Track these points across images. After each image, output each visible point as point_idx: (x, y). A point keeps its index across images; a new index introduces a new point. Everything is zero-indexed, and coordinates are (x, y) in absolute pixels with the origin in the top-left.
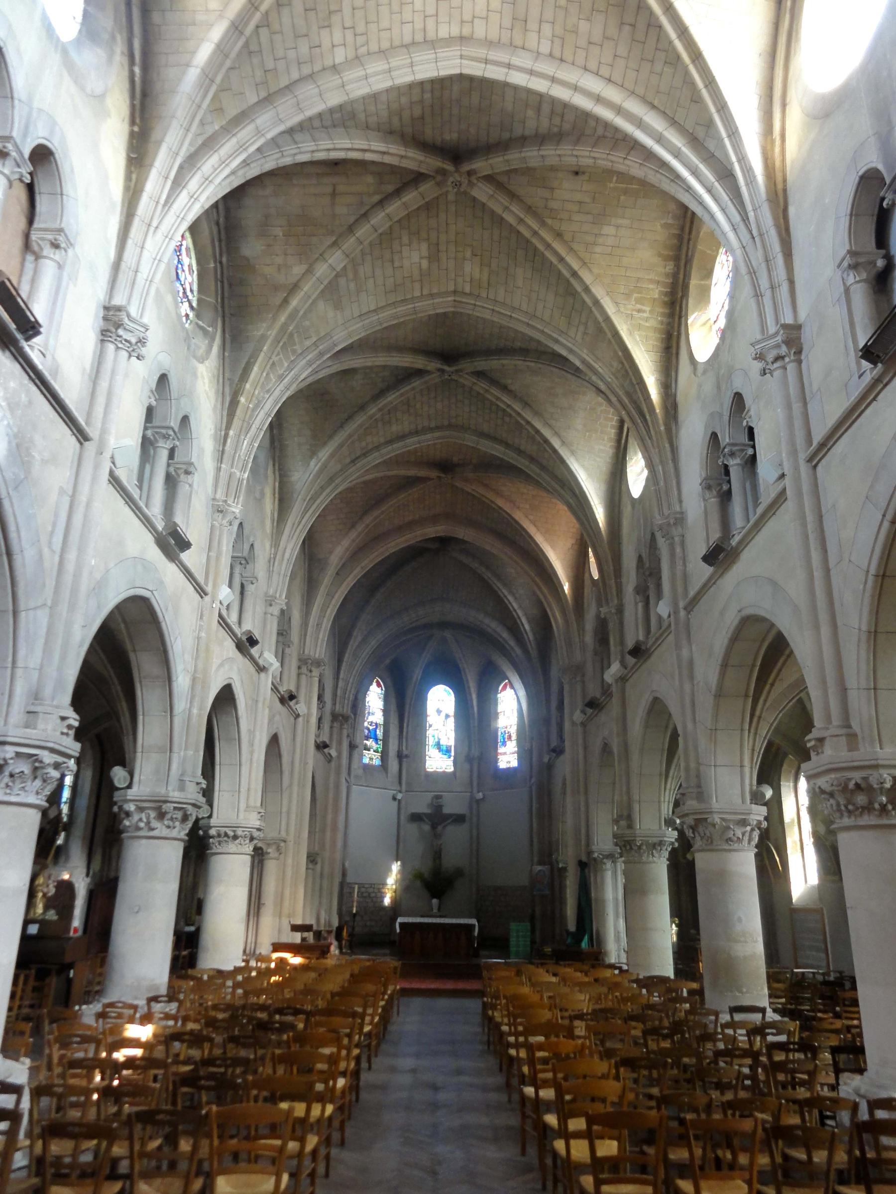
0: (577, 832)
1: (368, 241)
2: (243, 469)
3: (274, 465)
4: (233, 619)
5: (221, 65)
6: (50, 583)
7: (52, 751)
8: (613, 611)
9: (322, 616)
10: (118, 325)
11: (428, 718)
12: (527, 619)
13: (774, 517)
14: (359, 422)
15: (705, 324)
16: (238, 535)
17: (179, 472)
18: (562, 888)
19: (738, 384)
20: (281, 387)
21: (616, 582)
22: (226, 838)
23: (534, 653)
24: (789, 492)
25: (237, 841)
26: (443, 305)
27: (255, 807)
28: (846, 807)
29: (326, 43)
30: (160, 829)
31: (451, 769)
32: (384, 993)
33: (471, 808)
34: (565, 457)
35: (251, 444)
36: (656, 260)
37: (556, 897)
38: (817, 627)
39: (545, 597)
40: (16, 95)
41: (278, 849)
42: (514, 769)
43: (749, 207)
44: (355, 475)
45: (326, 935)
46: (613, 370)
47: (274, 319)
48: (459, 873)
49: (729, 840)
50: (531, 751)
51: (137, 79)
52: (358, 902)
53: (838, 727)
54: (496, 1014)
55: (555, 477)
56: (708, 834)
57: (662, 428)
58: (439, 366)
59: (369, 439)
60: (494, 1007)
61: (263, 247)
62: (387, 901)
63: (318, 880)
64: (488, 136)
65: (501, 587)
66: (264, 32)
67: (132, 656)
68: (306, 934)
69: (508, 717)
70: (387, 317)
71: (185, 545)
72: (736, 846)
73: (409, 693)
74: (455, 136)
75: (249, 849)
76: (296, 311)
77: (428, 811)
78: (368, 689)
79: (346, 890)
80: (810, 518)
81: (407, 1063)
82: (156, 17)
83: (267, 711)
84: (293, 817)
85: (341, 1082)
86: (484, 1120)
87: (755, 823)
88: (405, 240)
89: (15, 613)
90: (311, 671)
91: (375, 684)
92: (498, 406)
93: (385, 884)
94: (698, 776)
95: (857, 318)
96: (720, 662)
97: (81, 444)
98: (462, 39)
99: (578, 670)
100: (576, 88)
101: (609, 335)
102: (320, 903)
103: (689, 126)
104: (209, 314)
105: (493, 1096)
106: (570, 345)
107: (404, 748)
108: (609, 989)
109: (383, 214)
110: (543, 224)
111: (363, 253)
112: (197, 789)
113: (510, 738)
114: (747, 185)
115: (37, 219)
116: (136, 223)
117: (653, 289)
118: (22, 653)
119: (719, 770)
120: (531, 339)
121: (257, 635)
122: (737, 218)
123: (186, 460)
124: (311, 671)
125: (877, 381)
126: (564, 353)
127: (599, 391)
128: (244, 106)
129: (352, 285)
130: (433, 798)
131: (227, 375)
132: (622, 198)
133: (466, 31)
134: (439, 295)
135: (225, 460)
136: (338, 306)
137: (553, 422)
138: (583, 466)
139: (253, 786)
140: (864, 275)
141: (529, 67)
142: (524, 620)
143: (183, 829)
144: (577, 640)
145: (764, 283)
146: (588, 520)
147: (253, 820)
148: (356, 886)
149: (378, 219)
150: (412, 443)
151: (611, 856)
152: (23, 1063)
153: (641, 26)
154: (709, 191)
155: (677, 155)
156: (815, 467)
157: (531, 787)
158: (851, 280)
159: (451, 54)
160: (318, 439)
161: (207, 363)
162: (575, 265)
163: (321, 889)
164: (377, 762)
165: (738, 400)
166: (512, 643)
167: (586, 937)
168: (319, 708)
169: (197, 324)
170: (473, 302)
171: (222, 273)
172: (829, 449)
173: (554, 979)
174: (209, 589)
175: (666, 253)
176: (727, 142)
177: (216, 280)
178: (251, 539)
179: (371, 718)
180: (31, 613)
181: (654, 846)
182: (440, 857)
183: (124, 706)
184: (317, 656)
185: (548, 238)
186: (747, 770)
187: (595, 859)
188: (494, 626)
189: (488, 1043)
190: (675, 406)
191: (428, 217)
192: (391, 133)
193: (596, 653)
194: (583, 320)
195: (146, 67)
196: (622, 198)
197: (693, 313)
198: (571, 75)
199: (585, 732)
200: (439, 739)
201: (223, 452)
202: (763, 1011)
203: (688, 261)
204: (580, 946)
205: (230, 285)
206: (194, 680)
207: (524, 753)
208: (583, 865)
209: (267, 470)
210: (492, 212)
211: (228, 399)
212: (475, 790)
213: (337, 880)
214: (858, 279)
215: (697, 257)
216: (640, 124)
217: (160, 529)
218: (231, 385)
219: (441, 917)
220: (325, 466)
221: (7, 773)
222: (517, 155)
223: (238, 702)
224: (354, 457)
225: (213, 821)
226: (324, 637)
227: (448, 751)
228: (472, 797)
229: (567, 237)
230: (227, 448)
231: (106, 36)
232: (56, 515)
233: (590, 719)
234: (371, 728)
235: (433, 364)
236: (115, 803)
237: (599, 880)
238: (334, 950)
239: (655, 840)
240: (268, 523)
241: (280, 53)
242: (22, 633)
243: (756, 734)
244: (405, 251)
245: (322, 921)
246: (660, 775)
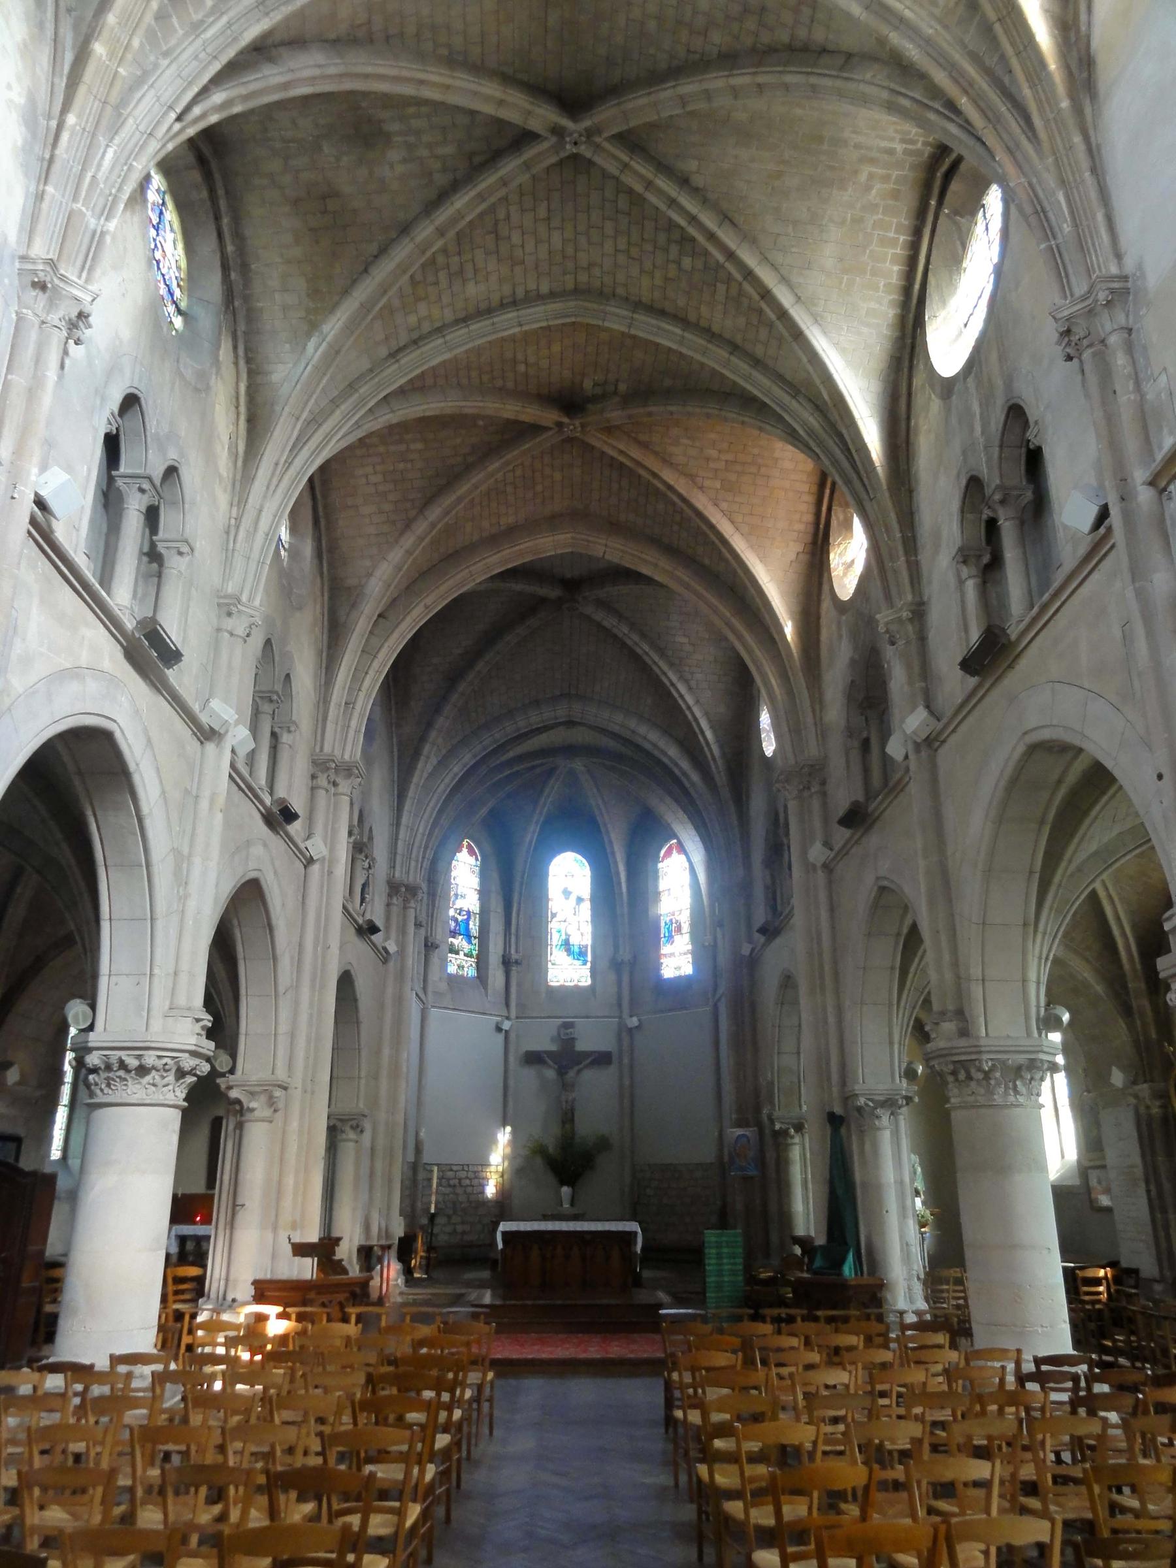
3: (235, 348)
8: (905, 614)
11: (550, 903)
12: (710, 721)
14: (397, 260)
22: (122, 1073)
23: (721, 778)
25: (148, 1078)
31: (586, 981)
33: (620, 1040)
34: (803, 326)
41: (271, 1102)
42: (688, 977)
46: (937, 12)
48: (603, 1144)
57: (1065, 104)
59: (423, 309)
62: (490, 1191)
63: (366, 1162)
65: (665, 668)
69: (677, 898)
71: (172, 656)
79: (421, 1175)
84: (301, 1043)
90: (335, 784)
91: (465, 850)
97: (202, 743)
102: (371, 1199)
107: (513, 951)
112: (197, 1028)
113: (679, 929)
124: (335, 784)
135: (53, 177)
137: (779, 258)
138: (836, 345)
139: (185, 966)
142: (704, 724)
144: (810, 720)
146: (847, 450)
148: (435, 1169)
151: (890, 1103)
157: (716, 1007)
163: (372, 1174)
164: (470, 972)
167: (850, 1257)
179: (459, 904)
182: (572, 1120)
184: (347, 757)
187: (859, 1110)
188: (653, 737)
199: (830, 883)
201: (51, 160)
204: (840, 1274)
207: (703, 951)
211: (69, 57)
219: (576, 1218)
223: (136, 779)
224: (394, 345)
227: (582, 954)
233: (844, 852)
234: (460, 918)
237: (868, 1147)
239: (1021, 1059)
245: (375, 1230)
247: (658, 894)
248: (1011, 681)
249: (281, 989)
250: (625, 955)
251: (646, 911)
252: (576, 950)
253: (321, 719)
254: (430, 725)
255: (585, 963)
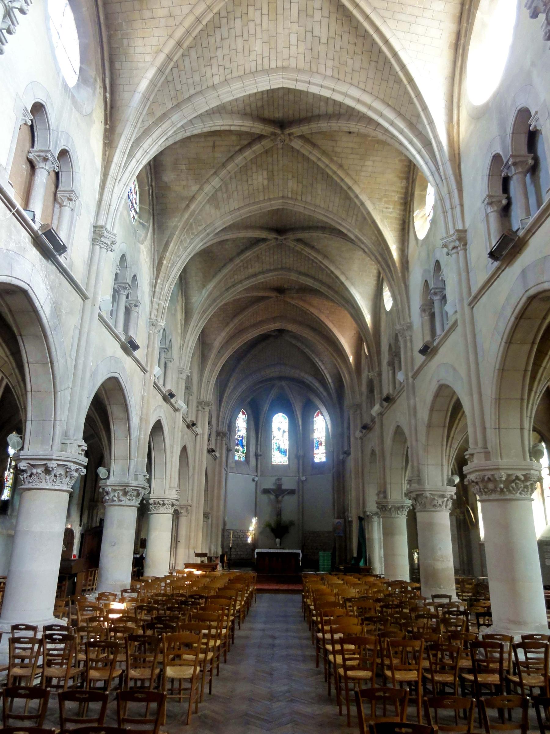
0: (358, 500)
1: (234, 171)
2: (166, 301)
3: (182, 293)
4: (160, 383)
5: (153, 90)
6: (71, 376)
7: (75, 463)
8: (376, 375)
9: (210, 377)
10: (101, 236)
13: (454, 332)
15: (423, 217)
16: (163, 336)
17: (131, 305)
18: (351, 531)
19: (438, 256)
20: (186, 254)
21: (378, 359)
23: (334, 395)
24: (459, 322)
25: (165, 507)
26: (277, 204)
27: (174, 487)
28: (483, 490)
29: (209, 74)
30: (125, 501)
31: (286, 463)
32: (247, 590)
35: (170, 287)
36: (396, 179)
37: (346, 537)
38: (471, 395)
39: (339, 364)
40: (51, 128)
41: (187, 510)
42: (324, 462)
43: (440, 164)
44: (229, 297)
45: (214, 559)
47: (182, 216)
48: (292, 523)
49: (435, 505)
50: (333, 452)
51: (108, 100)
52: (233, 541)
53: (481, 448)
54: (308, 601)
55: (343, 297)
56: (423, 503)
57: (400, 275)
58: (275, 236)
59: (236, 277)
60: (307, 597)
61: (175, 176)
62: (250, 540)
64: (299, 114)
66: (175, 70)
67: (108, 408)
68: (203, 559)
70: (245, 213)
71: (62, 249)
72: (438, 509)
73: (261, 417)
74: (281, 115)
75: (171, 511)
76: (194, 211)
77: (274, 487)
78: (237, 416)
79: (226, 534)
80: (469, 336)
81: (260, 626)
82: (117, 65)
83: (180, 433)
84: (195, 492)
85: (224, 631)
86: (299, 652)
87: (449, 496)
88: (254, 169)
89: (55, 393)
90: (204, 409)
91: (241, 413)
92: (309, 257)
93: (248, 530)
94: (419, 471)
95: (492, 231)
96: (429, 408)
97: (84, 301)
98: (283, 68)
99: (358, 406)
100: (346, 95)
101: (370, 221)
103: (408, 116)
104: (145, 215)
105: (305, 642)
106: (348, 227)
108: (370, 587)
109: (242, 157)
110: (332, 160)
111: (231, 178)
112: (144, 479)
113: (321, 444)
114: (439, 151)
115: (60, 185)
116: (109, 178)
117: (394, 196)
118: (59, 413)
119: (429, 467)
120: (326, 223)
121: (174, 392)
122: (434, 169)
123: (135, 299)
124: (204, 409)
125: (498, 268)
126: (345, 231)
127: (364, 251)
128: (165, 110)
129: (225, 196)
130: (276, 480)
131: (156, 248)
132: (376, 145)
133: (286, 64)
134: (274, 199)
135: (156, 296)
136: (217, 207)
139: (173, 476)
140: (496, 208)
141: (321, 83)
143: (137, 501)
144: (357, 390)
145: (448, 206)
147: (173, 495)
149: (239, 159)
150: (261, 279)
152: (65, 620)
153: (381, 63)
154: (419, 152)
155: (402, 132)
156: (472, 308)
158: (489, 210)
159: (277, 77)
160: (207, 278)
161: (145, 243)
162: (350, 183)
164: (243, 459)
165: (438, 263)
166: (321, 389)
168: (209, 429)
169: (139, 221)
170: (293, 203)
171: (153, 192)
172: (479, 300)
173: (341, 582)
174: (148, 369)
175: (401, 175)
176: (428, 127)
177: (149, 195)
178: (170, 337)
179: (239, 433)
180: (63, 392)
181: (399, 508)
183: (103, 434)
185: (334, 168)
186: (445, 468)
187: (368, 516)
188: (309, 379)
189: (305, 617)
190: (407, 262)
191: (267, 157)
192: (245, 114)
193: (368, 397)
194: (356, 213)
195: (112, 93)
196: (376, 145)
197: (417, 210)
198: (343, 88)
200: (279, 445)
201: (155, 291)
202: (450, 597)
203: (414, 181)
204: (358, 565)
205: (157, 198)
206: (141, 419)
208: (361, 519)
209: (178, 296)
210: (303, 155)
212: (301, 475)
213: (221, 527)
214: (492, 210)
215: (418, 178)
216: (381, 115)
217: (123, 339)
218: (158, 254)
220: (210, 293)
221: (53, 475)
222: (316, 126)
223: (164, 429)
225: (151, 496)
226: (211, 388)
227: (285, 452)
228: (299, 479)
229: (346, 167)
230: (157, 290)
231: (92, 80)
232: (73, 339)
233: (365, 436)
234: (239, 439)
235: (271, 236)
236: (100, 487)
237: (370, 528)
238: (219, 567)
239: (399, 505)
240: (179, 326)
241: (184, 81)
242: (58, 403)
243: (451, 447)
244: (254, 176)
246: (402, 468)
247: (313, 430)
248: (395, 405)
249: (190, 476)
250: (301, 453)
251: (309, 436)
252: (283, 450)
253: (200, 388)
254: (231, 376)
255: (286, 456)
